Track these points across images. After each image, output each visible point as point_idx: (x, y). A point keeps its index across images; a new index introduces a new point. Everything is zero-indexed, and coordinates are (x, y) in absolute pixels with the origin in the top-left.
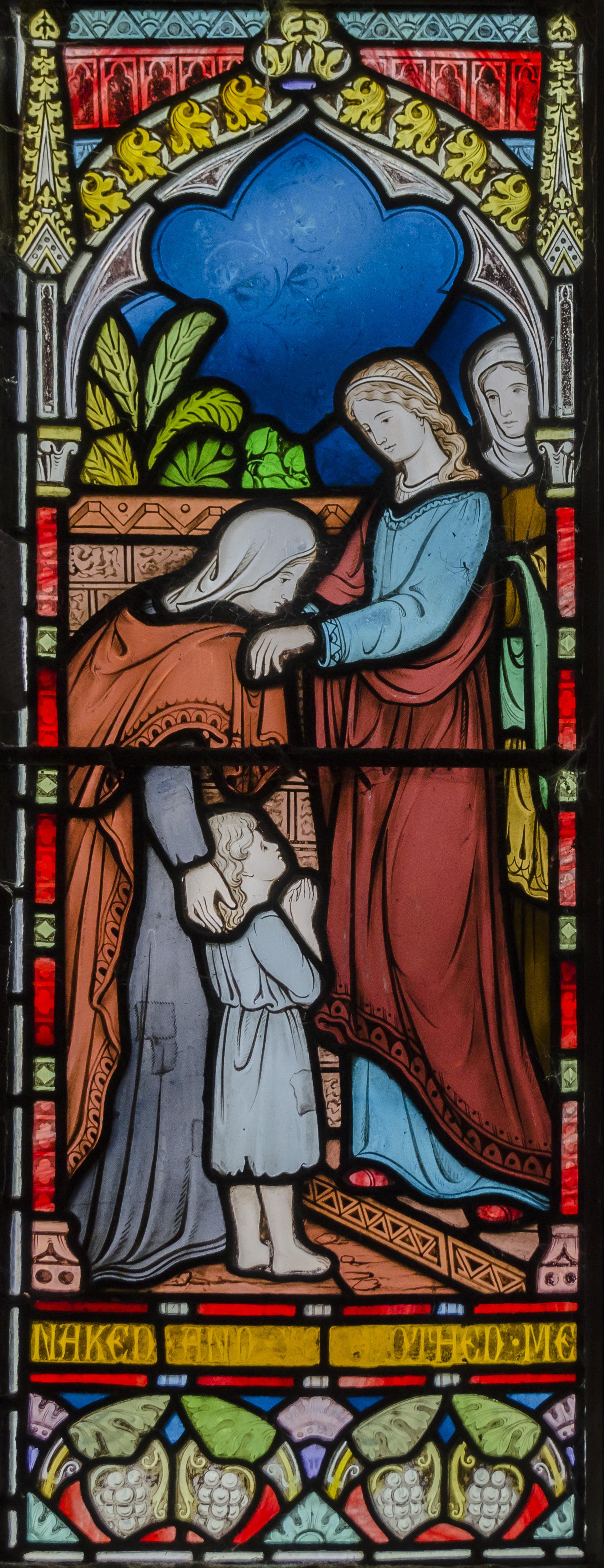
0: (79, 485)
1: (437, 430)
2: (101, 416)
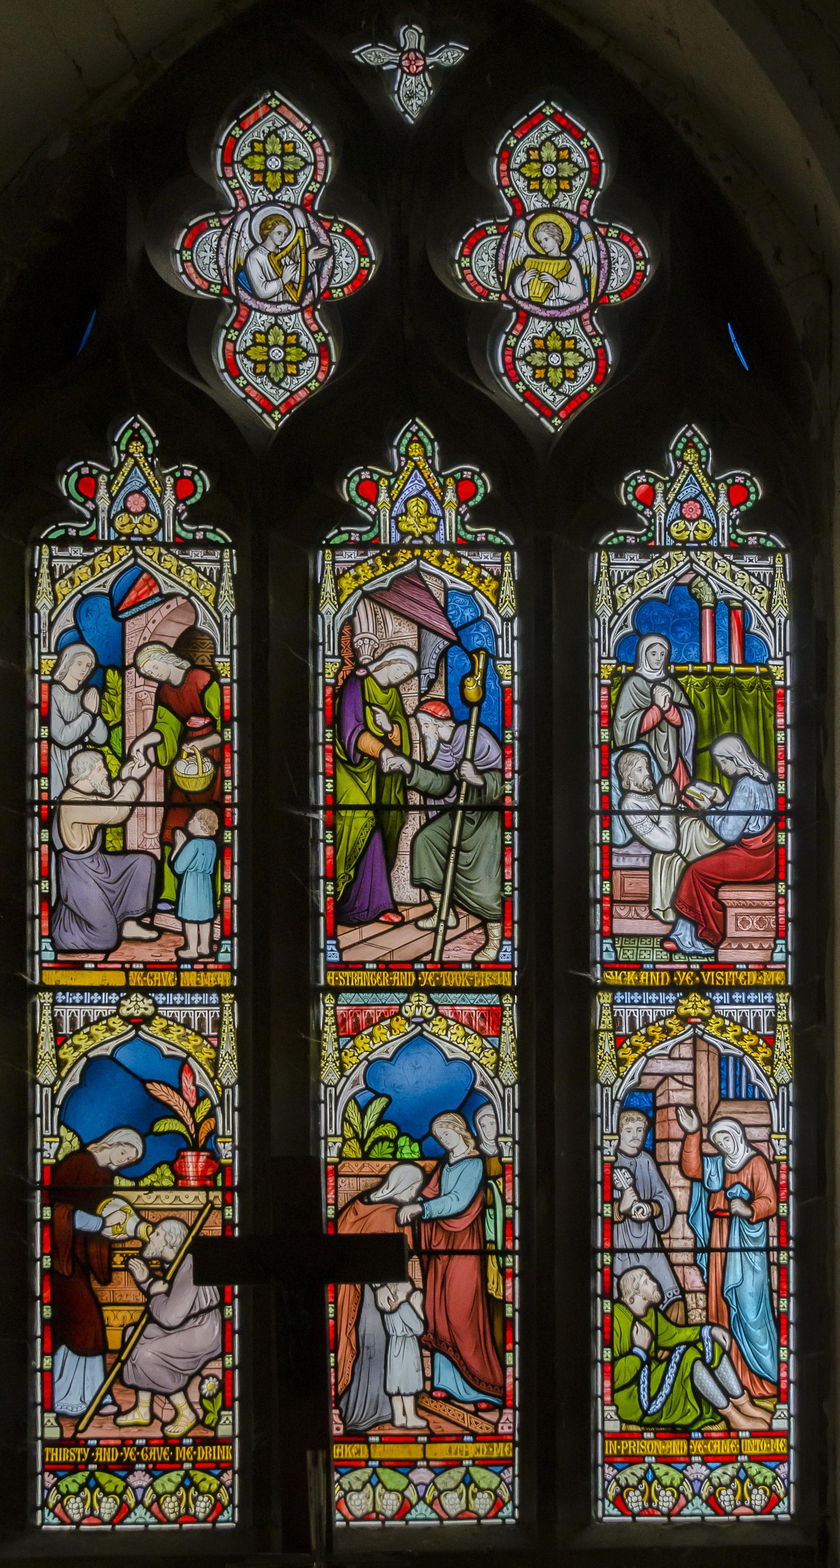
0: (341, 1157)
1: (464, 1138)
2: (349, 1134)
